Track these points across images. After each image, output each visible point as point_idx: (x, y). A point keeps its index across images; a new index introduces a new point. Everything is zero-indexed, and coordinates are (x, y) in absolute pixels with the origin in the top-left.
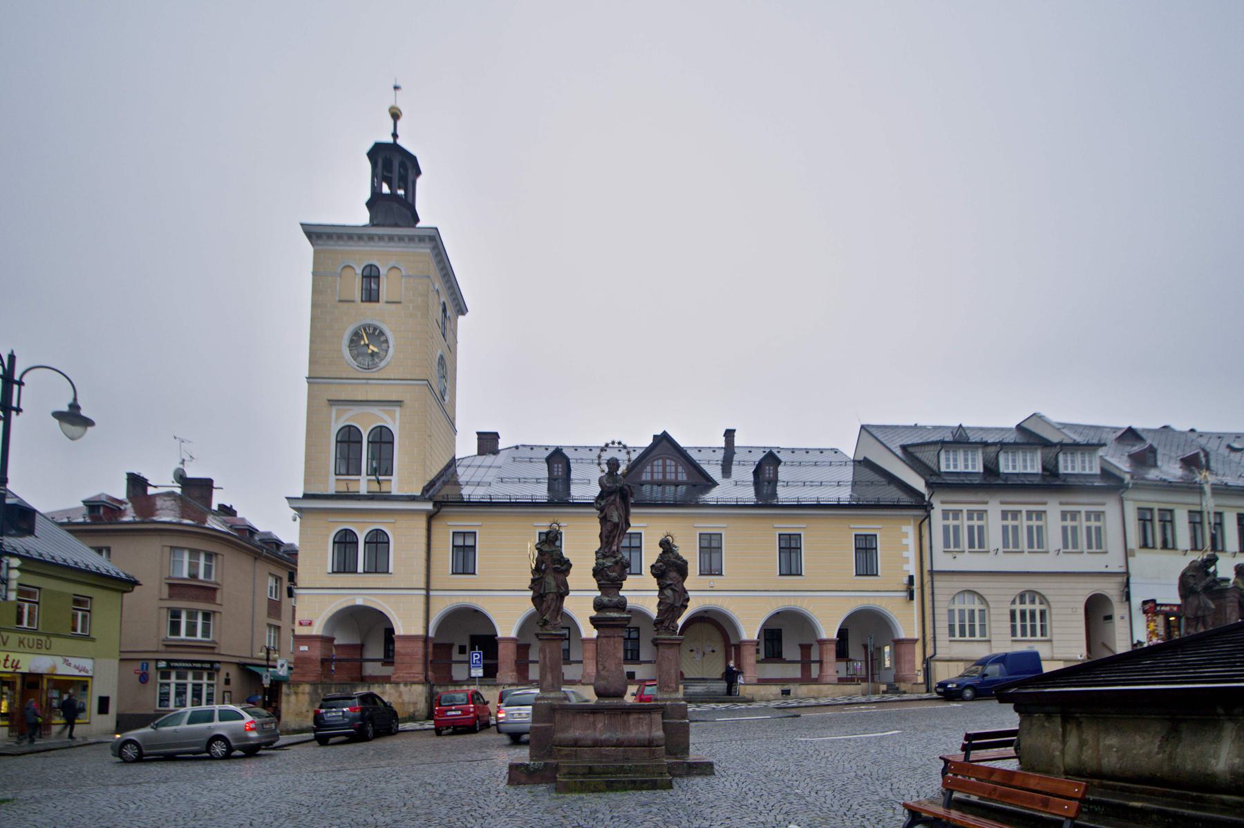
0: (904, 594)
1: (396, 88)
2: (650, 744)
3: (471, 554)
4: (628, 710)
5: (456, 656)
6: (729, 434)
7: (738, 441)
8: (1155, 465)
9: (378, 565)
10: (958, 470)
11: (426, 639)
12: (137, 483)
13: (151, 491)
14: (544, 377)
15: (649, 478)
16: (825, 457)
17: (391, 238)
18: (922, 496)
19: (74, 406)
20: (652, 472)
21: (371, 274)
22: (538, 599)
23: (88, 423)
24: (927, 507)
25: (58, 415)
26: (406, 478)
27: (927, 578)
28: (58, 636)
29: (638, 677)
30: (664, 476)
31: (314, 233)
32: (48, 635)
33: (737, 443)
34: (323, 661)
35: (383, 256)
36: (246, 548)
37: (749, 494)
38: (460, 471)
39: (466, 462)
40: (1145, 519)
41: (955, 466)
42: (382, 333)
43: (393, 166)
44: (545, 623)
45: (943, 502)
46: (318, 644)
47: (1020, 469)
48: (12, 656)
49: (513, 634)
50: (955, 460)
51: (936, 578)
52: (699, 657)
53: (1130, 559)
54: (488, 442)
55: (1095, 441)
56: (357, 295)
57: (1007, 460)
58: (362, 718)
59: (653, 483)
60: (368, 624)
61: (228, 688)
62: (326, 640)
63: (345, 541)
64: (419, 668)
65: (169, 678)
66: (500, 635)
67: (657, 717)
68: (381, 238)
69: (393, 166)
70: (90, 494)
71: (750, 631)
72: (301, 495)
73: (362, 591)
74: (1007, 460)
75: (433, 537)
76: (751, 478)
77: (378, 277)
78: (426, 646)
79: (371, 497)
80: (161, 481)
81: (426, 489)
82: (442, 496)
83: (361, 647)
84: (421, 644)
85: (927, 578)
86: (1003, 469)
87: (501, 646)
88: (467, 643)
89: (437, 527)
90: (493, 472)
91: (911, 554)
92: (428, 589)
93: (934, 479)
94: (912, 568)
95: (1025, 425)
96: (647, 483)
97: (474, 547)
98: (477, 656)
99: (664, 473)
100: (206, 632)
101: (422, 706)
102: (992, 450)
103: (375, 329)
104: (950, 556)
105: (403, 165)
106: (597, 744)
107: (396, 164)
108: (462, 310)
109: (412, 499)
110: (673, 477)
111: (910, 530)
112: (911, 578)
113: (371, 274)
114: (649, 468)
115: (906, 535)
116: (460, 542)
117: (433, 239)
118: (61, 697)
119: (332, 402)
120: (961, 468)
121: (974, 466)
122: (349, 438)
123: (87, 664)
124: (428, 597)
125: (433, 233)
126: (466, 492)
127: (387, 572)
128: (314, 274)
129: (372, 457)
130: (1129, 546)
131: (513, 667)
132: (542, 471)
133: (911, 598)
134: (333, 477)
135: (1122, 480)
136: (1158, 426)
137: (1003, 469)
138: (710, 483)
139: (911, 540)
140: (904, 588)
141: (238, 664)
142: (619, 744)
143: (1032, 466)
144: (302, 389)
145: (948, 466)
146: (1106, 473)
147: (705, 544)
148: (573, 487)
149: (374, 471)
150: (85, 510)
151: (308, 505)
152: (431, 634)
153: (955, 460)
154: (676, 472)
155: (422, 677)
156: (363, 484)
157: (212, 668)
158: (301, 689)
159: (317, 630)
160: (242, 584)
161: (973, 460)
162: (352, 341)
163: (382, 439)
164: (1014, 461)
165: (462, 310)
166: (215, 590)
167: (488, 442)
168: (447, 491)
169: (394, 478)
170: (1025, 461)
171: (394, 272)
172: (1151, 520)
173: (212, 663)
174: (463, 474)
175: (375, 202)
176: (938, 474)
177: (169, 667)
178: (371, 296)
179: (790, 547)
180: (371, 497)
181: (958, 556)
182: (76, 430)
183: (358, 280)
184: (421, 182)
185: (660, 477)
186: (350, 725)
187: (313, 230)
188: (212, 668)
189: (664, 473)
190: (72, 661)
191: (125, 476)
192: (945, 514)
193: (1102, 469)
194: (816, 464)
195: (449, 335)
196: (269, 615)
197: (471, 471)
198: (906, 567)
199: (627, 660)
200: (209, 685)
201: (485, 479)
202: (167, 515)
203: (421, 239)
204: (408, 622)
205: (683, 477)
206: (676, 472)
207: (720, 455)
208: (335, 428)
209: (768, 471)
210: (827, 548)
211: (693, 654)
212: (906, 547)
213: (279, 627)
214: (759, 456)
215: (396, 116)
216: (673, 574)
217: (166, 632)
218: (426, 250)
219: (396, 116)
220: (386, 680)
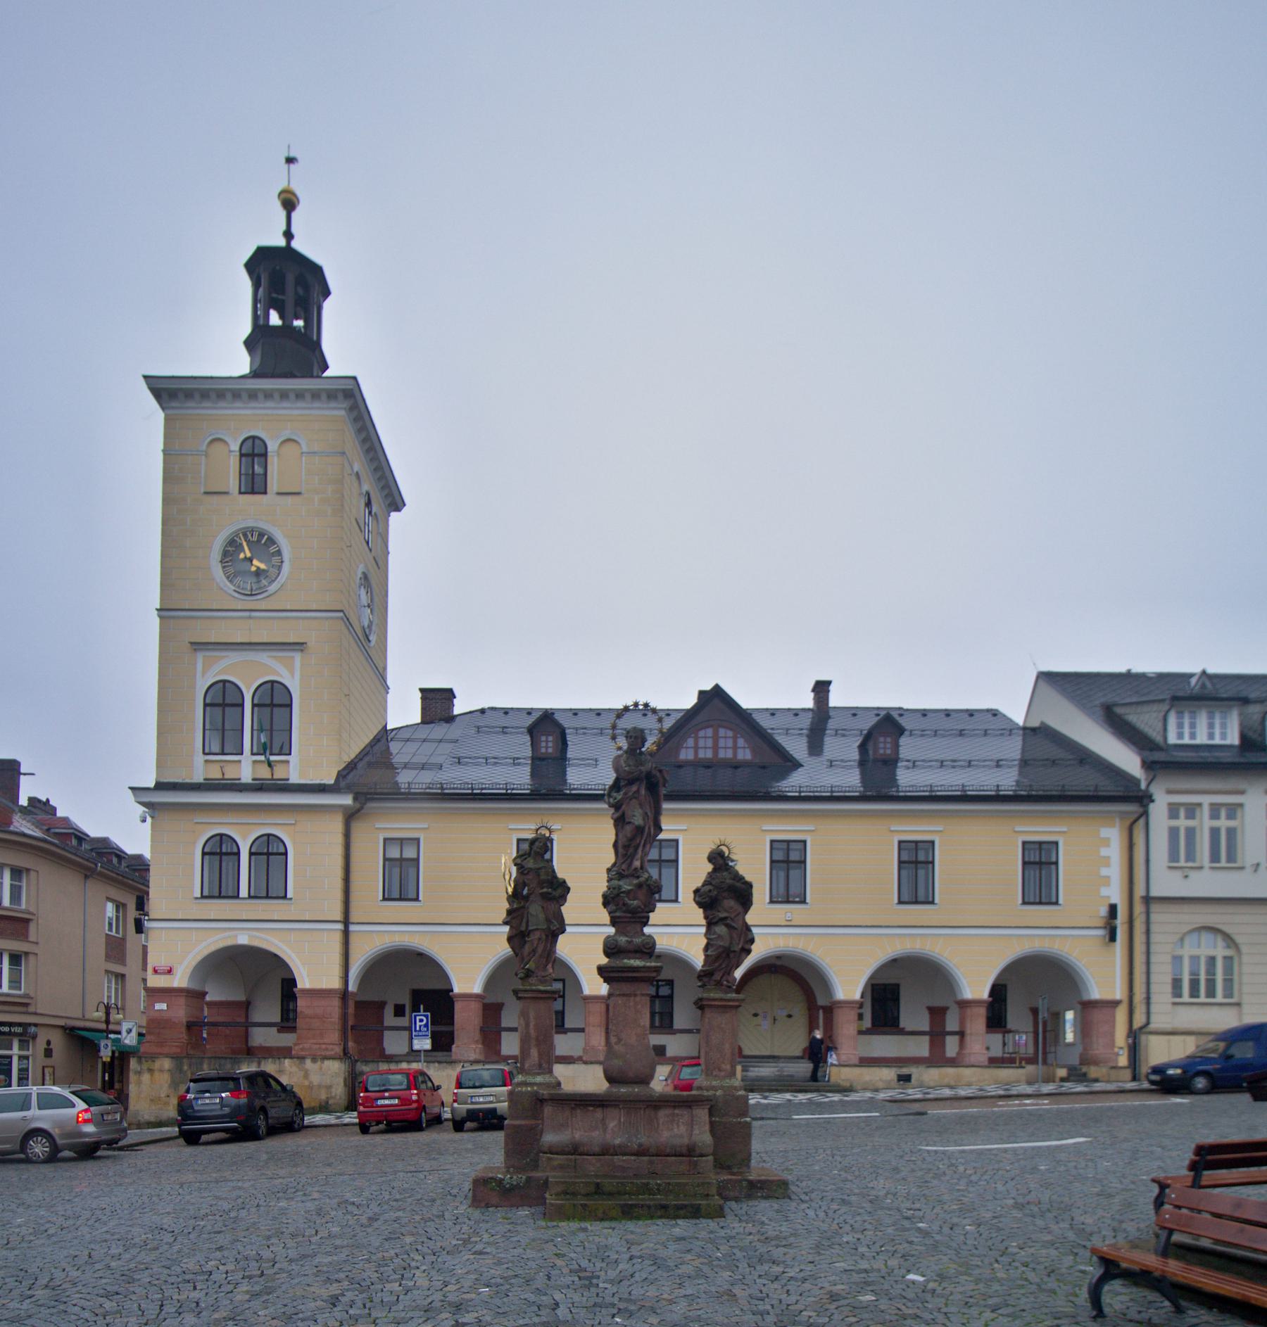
0: (1101, 932)
1: (290, 160)
2: (690, 1152)
5: (389, 1019)
6: (821, 688)
7: (836, 699)
9: (271, 887)
10: (1198, 741)
11: (344, 995)
17: (284, 395)
18: (1136, 782)
20: (696, 748)
21: (254, 452)
24: (1144, 799)
26: (314, 755)
27: (1139, 908)
31: (166, 391)
33: (832, 703)
34: (190, 1026)
37: (851, 779)
38: (394, 747)
39: (402, 735)
42: (271, 541)
44: (528, 974)
45: (1169, 792)
46: (182, 1001)
49: (477, 988)
50: (1193, 726)
51: (1154, 907)
52: (766, 1024)
54: (437, 703)
56: (233, 483)
62: (194, 996)
63: (220, 852)
64: (334, 1036)
66: (456, 990)
67: (702, 1114)
68: (268, 395)
69: (288, 283)
71: (848, 985)
72: (152, 785)
79: (259, 787)
81: (341, 775)
83: (246, 1006)
85: (1139, 908)
87: (458, 1006)
88: (406, 1001)
89: (358, 829)
90: (446, 748)
91: (1115, 872)
92: (346, 922)
93: (1158, 756)
99: (716, 748)
101: (339, 1092)
103: (261, 535)
104: (1178, 874)
105: (301, 281)
106: (606, 1151)
107: (290, 279)
108: (396, 503)
109: (321, 789)
111: (1111, 837)
112: (1113, 909)
113: (254, 452)
114: (690, 742)
115: (1106, 843)
116: (394, 853)
117: (349, 395)
120: (1202, 739)
122: (223, 700)
124: (346, 933)
125: (349, 385)
126: (404, 778)
129: (258, 729)
131: (477, 1036)
133: (1113, 938)
134: (200, 759)
140: (1101, 923)
142: (641, 1152)
145: (1180, 736)
147: (779, 856)
151: (162, 799)
152: (352, 987)
154: (735, 748)
155: (338, 1050)
156: (246, 768)
158: (157, 1064)
159: (180, 980)
162: (225, 554)
163: (275, 700)
165: (396, 503)
166: (27, 921)
167: (437, 703)
169: (293, 759)
173: (25, 1026)
175: (259, 339)
178: (254, 484)
180: (259, 787)
181: (1193, 874)
183: (234, 462)
192: (1173, 811)
196: (108, 957)
197: (411, 747)
198: (1104, 892)
199: (654, 1028)
200: (20, 1057)
201: (433, 760)
204: (317, 968)
205: (745, 754)
206: (735, 748)
207: (806, 721)
211: (759, 1020)
212: (1106, 861)
215: (289, 203)
216: (730, 903)
218: (338, 412)
219: (289, 203)
220: (285, 1053)
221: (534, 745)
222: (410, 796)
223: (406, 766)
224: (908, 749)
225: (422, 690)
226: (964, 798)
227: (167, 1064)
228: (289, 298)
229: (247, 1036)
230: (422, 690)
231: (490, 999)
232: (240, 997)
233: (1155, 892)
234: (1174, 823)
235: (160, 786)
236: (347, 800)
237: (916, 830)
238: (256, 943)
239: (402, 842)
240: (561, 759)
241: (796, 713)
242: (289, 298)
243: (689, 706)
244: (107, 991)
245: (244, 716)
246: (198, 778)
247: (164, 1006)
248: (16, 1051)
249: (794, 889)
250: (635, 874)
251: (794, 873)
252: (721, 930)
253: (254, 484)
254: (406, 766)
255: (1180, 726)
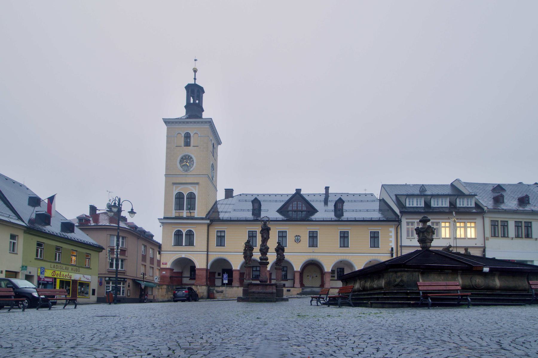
1: (195, 60)
2: (272, 293)
3: (223, 239)
4: (267, 285)
5: (217, 276)
6: (327, 188)
7: (330, 191)
8: (503, 202)
9: (190, 243)
10: (414, 206)
11: (207, 270)
12: (93, 209)
13: (98, 212)
14: (251, 169)
15: (291, 209)
16: (367, 197)
17: (195, 122)
18: (398, 216)
19: (132, 210)
20: (292, 207)
21: (187, 136)
22: (245, 257)
23: (135, 213)
24: (399, 221)
25: (129, 212)
26: (200, 211)
27: (399, 249)
28: (82, 267)
29: (286, 286)
30: (297, 208)
31: (167, 122)
32: (79, 267)
33: (330, 192)
34: (170, 277)
35: (192, 129)
36: (134, 234)
37: (331, 215)
38: (219, 206)
39: (221, 202)
40: (494, 224)
41: (413, 204)
42: (191, 158)
43: (195, 92)
44: (247, 263)
46: (169, 271)
47: (440, 205)
48: (70, 274)
49: (238, 268)
50: (413, 202)
51: (403, 248)
52: (310, 278)
53: (486, 241)
54: (229, 193)
55: (473, 194)
56: (183, 144)
57: (434, 202)
58: (189, 294)
59: (292, 211)
60: (187, 265)
61: (129, 288)
62: (171, 270)
63: (178, 234)
64: (204, 280)
65: (109, 284)
66: (233, 269)
67: (274, 287)
68: (191, 122)
69: (195, 92)
70: (79, 214)
71: (328, 268)
72: (162, 218)
73: (184, 253)
74: (434, 202)
75: (210, 233)
76: (333, 208)
77: (190, 137)
78: (207, 273)
79: (187, 218)
80: (102, 208)
81: (207, 215)
82: (213, 218)
83: (181, 273)
84: (205, 272)
85: (399, 249)
86: (432, 205)
87: (234, 273)
88: (221, 272)
89: (211, 229)
90: (231, 206)
91: (393, 239)
92: (208, 251)
93: (404, 210)
94: (393, 245)
95: (454, 184)
96: (290, 211)
97: (224, 236)
98: (225, 276)
99: (297, 207)
100: (122, 267)
101: (205, 294)
102: (429, 197)
103: (189, 156)
104: (409, 240)
105: (198, 91)
106: (259, 293)
107: (196, 91)
108: (219, 143)
109: (202, 219)
110: (301, 208)
111: (392, 230)
112: (392, 248)
113: (187, 136)
114: (291, 205)
115: (391, 232)
116: (219, 234)
117: (210, 122)
118: (81, 289)
119: (174, 184)
120: (415, 205)
121: (420, 204)
122: (179, 197)
123: (89, 277)
124: (207, 254)
125: (210, 120)
126: (221, 216)
127: (193, 245)
128: (167, 136)
129: (187, 204)
130: (486, 236)
131: (238, 280)
132: (250, 206)
134: (174, 211)
135: (483, 209)
136: (516, 182)
137: (433, 205)
138: (315, 211)
139: (393, 233)
140: (390, 252)
141: (132, 279)
142: (264, 293)
143: (445, 204)
144: (164, 178)
145: (409, 204)
146: (478, 206)
147: (311, 235)
148: (262, 212)
149: (188, 209)
150: (77, 220)
151: (166, 221)
152: (209, 268)
153: (413, 202)
154: (302, 207)
155: (205, 283)
156: (185, 214)
157: (124, 281)
158: (163, 287)
159: (168, 266)
160: (135, 248)
161: (420, 202)
162: (180, 161)
163: (192, 197)
164: (437, 202)
165: (219, 143)
166: (125, 251)
167: (229, 193)
168: (214, 216)
169: (196, 211)
170: (442, 202)
171: (196, 135)
172: (497, 225)
173: (124, 278)
174: (220, 208)
175: (188, 106)
176: (405, 207)
177: (110, 280)
178: (187, 144)
179: (344, 237)
180: (187, 218)
181: (412, 240)
182: (133, 215)
183: (183, 139)
184: (205, 96)
185: (296, 208)
186: (185, 297)
187: (167, 120)
188: (124, 281)
189: (297, 207)
190: (85, 276)
191: (89, 207)
192: (408, 223)
193: (476, 204)
194: (362, 201)
195: (215, 155)
196: (142, 260)
197: (223, 206)
198: (391, 244)
199: (283, 280)
200: (123, 287)
201: (228, 210)
202: (104, 221)
203: (206, 122)
204: (200, 263)
205: (304, 208)
206: (302, 207)
207: (323, 198)
208: (175, 193)
209: (339, 205)
210: (359, 238)
211: (309, 277)
212: (391, 237)
213: (145, 266)
214: (337, 198)
215: (195, 71)
216: (281, 251)
217: (108, 267)
218: (207, 126)
219: (195, 71)
220: (193, 285)
221: (253, 205)
222: (223, 221)
223: (222, 212)
224: (346, 206)
225: (225, 189)
226: (355, 221)
227: (165, 287)
228: (196, 95)
229: (181, 281)
230: (225, 189)
231: (242, 272)
232: (180, 271)
233: (403, 245)
234: (408, 227)
235: (165, 218)
236: (208, 222)
237: (344, 229)
238: (187, 257)
239: (221, 231)
240: (260, 210)
241: (320, 195)
242: (196, 95)
243: (294, 193)
244: (142, 270)
245: (183, 201)
246: (174, 216)
247: (164, 272)
248: (122, 285)
249: (315, 243)
250: (265, 246)
251: (315, 239)
252: (279, 256)
253: (187, 144)
254: (222, 212)
255: (409, 202)
